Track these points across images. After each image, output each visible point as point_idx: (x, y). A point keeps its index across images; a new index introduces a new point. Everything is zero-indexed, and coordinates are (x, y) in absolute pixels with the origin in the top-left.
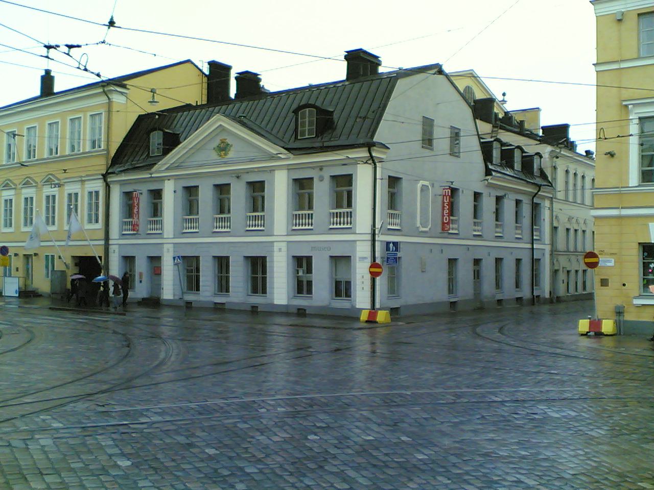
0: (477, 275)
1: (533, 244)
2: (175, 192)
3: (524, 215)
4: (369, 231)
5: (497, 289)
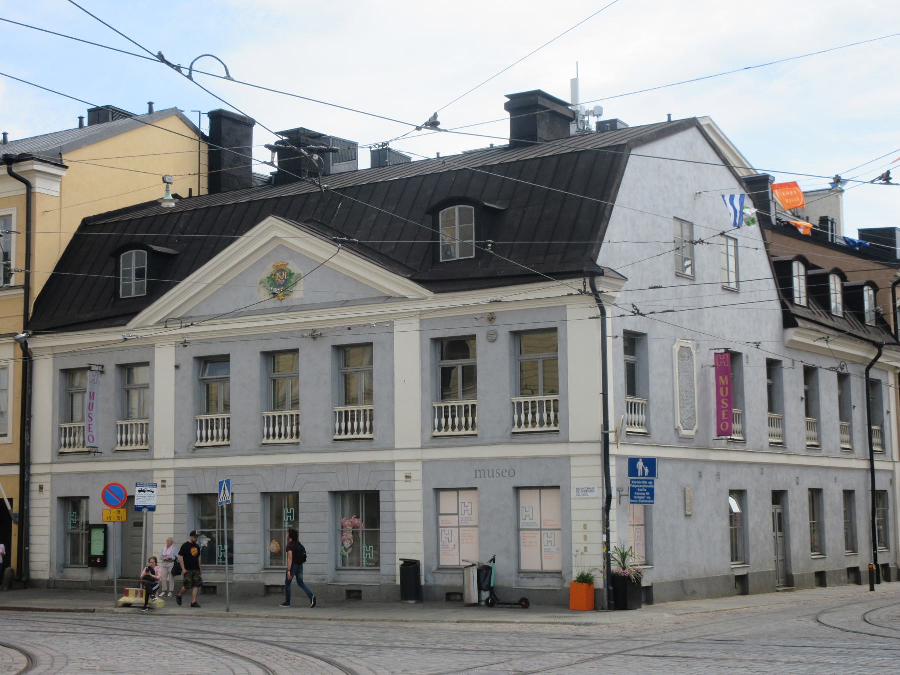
0: (781, 523)
1: (872, 461)
2: (177, 367)
3: (853, 404)
4: (599, 437)
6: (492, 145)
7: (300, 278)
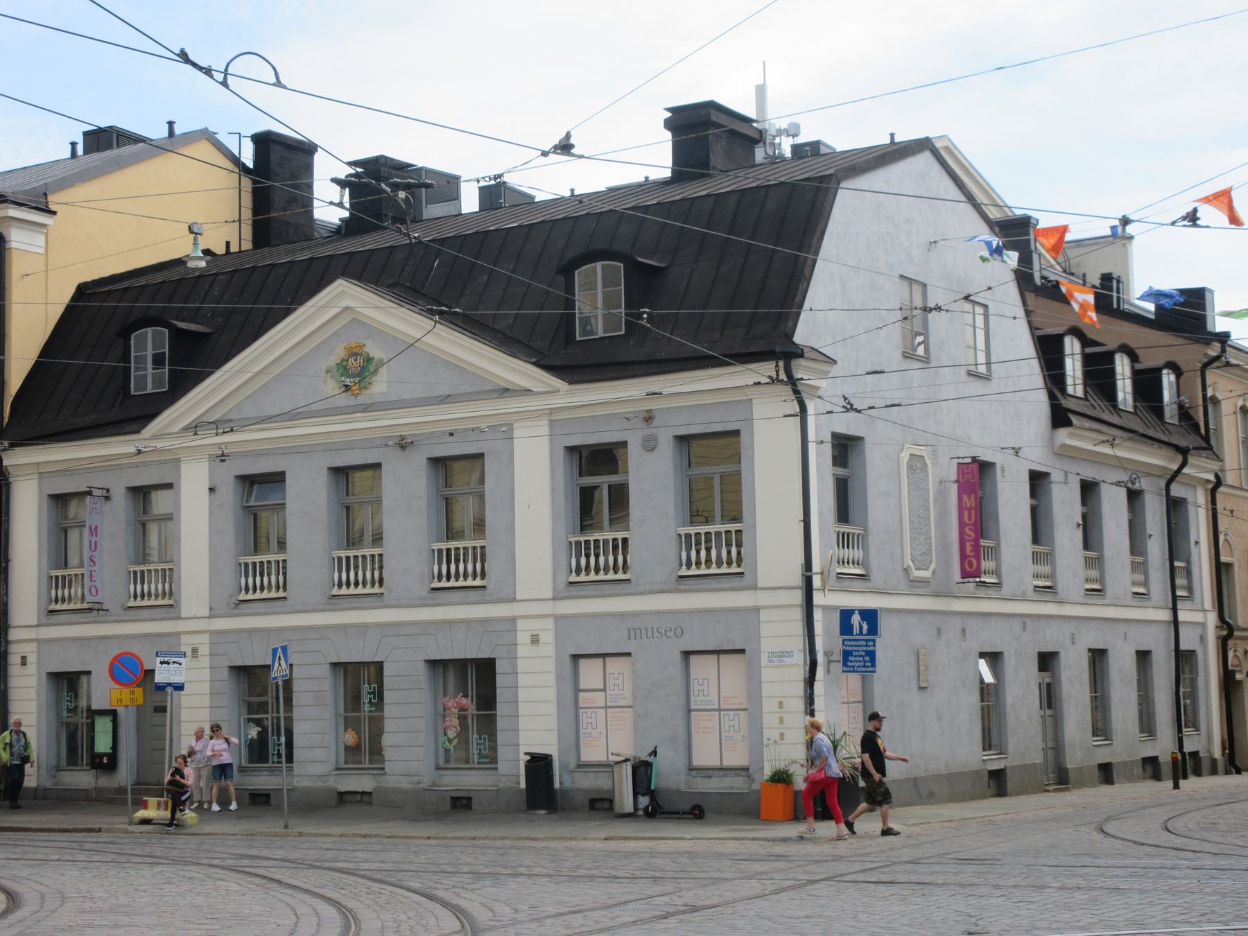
0: (1050, 697)
2: (212, 490)
3: (1149, 531)
4: (797, 580)
5: (984, 750)
6: (647, 178)
7: (381, 364)
